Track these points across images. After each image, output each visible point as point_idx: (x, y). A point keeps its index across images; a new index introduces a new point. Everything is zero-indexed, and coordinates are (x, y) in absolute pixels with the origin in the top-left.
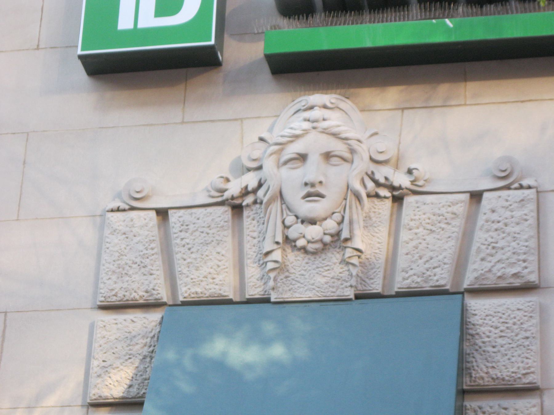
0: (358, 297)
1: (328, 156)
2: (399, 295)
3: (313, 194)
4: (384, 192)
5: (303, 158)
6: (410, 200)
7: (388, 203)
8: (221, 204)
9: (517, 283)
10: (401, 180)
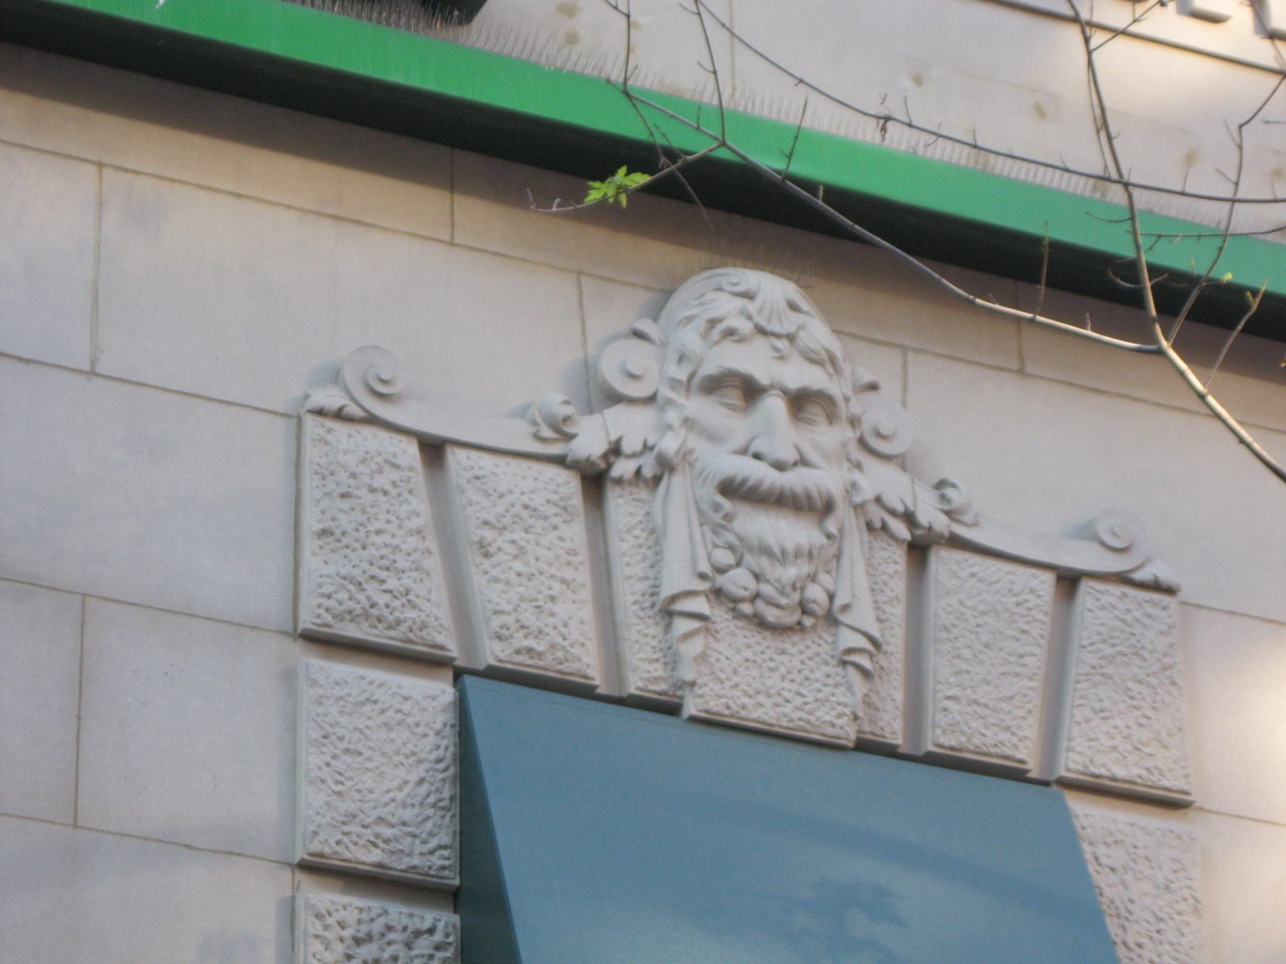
8: (560, 461)
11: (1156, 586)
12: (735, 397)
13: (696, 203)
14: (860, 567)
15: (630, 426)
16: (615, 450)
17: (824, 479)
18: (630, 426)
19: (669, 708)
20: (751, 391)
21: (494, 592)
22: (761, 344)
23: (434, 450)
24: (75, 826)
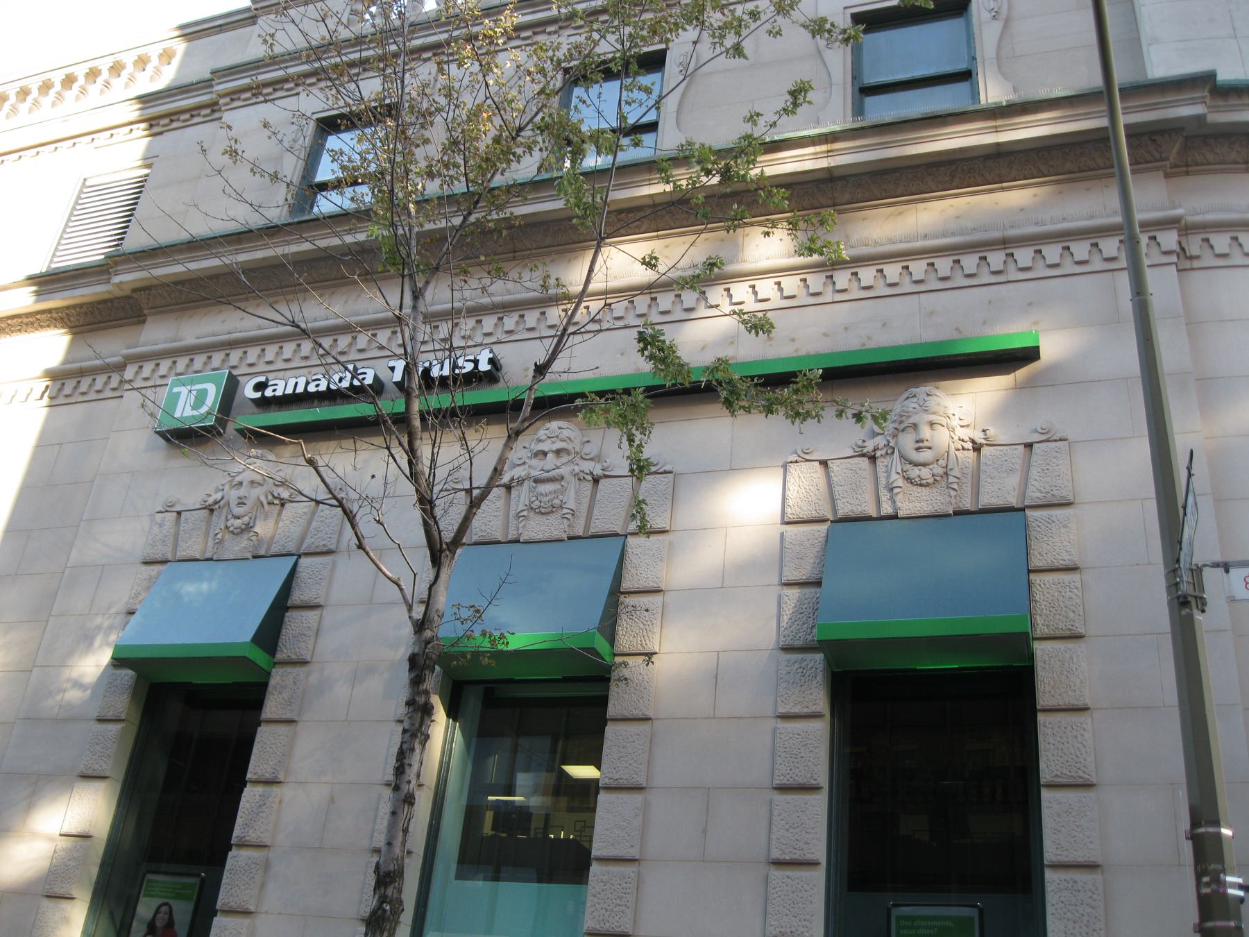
0: (1023, 510)
1: (252, 482)
2: (273, 556)
3: (241, 504)
4: (277, 502)
5: (241, 483)
6: (602, 481)
7: (278, 507)
8: (863, 455)
9: (325, 549)
10: (285, 494)
11: (665, 472)
12: (541, 456)
14: (573, 492)
16: (513, 479)
19: (518, 541)
20: (545, 454)
22: (549, 441)
23: (824, 463)
24: (1029, 571)
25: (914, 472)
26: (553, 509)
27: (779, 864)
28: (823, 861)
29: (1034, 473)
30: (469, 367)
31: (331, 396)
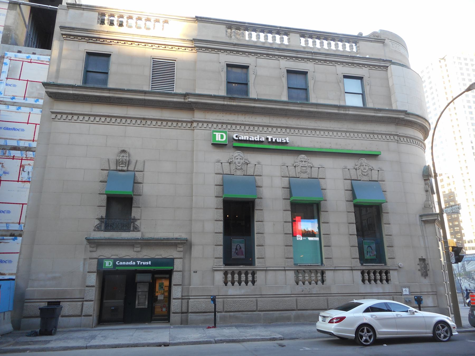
13: (98, 228)
15: (297, 164)
17: (306, 165)
18: (297, 164)
21: (290, 173)
23: (222, 163)
25: (363, 173)
26: (306, 172)
27: (351, 235)
28: (255, 234)
29: (380, 175)
30: (285, 141)
31: (255, 142)
